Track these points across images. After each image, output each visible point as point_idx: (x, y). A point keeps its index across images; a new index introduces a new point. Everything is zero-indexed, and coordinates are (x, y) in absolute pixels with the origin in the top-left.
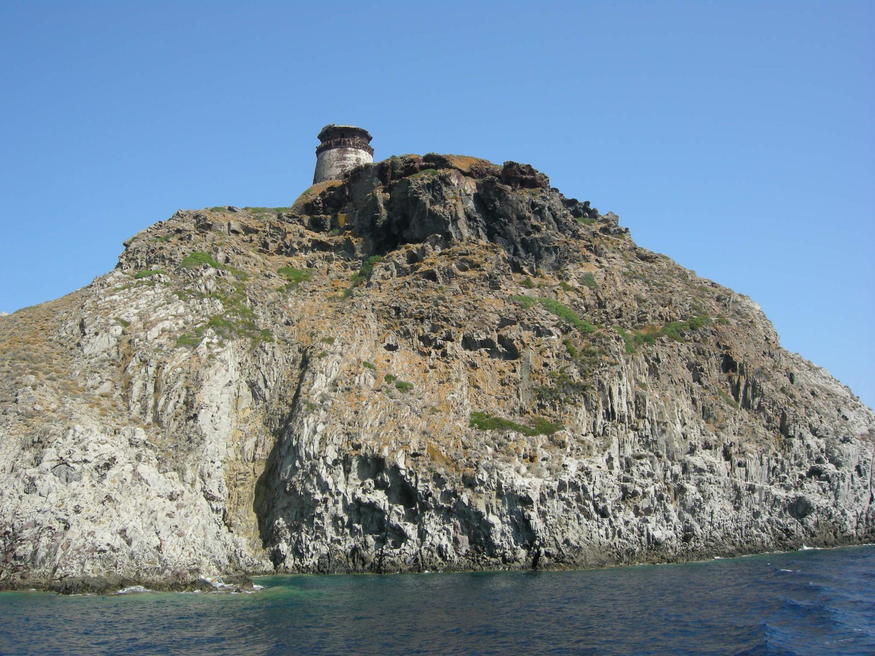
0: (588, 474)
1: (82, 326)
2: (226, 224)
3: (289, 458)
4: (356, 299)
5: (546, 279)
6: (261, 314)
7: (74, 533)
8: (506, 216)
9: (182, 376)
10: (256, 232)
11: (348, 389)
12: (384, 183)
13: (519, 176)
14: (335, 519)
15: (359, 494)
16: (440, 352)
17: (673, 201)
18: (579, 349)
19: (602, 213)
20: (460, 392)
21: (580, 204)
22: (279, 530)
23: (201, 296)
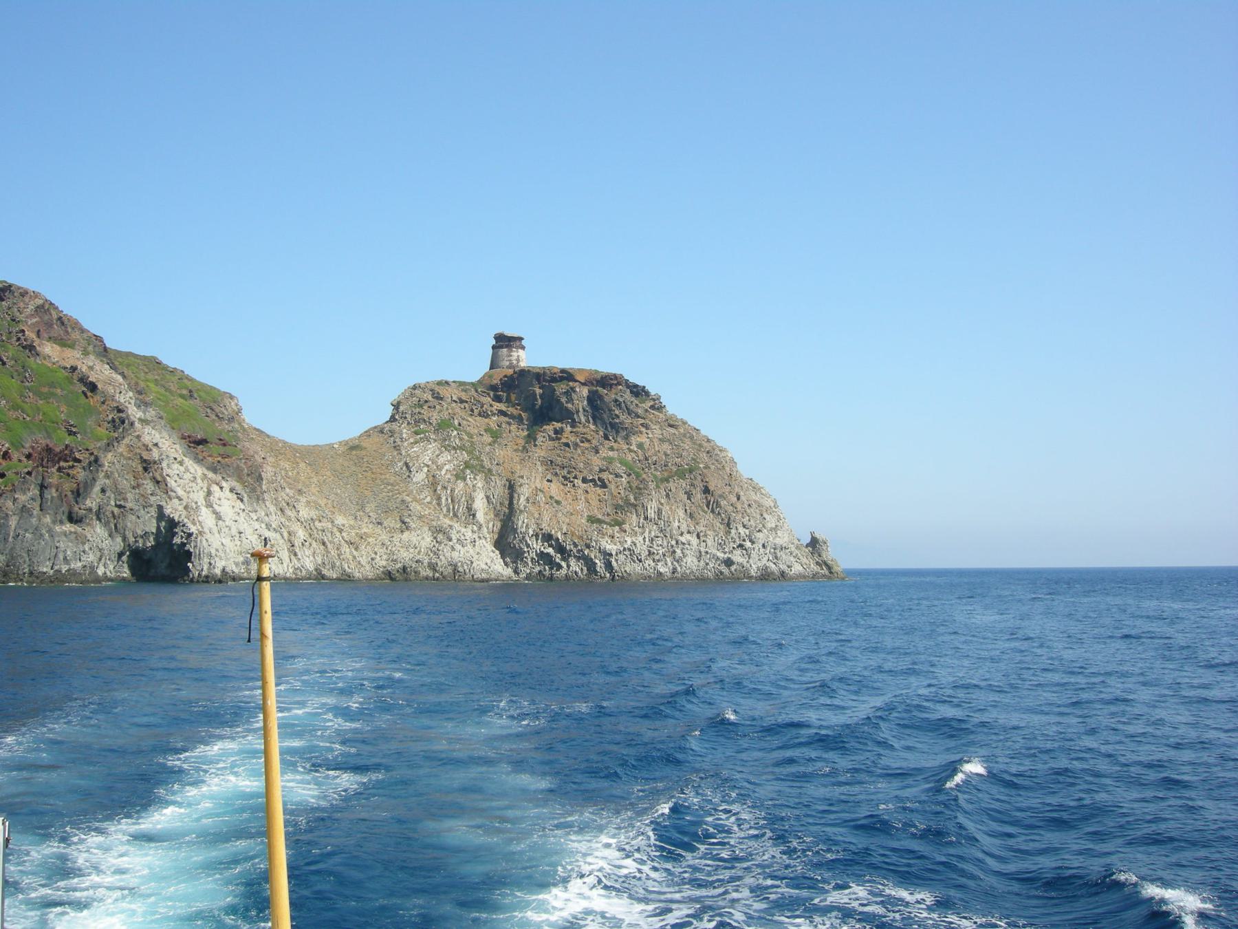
1: (406, 464)
13: (608, 381)
17: (695, 386)
18: (634, 486)
19: (653, 392)
20: (581, 506)
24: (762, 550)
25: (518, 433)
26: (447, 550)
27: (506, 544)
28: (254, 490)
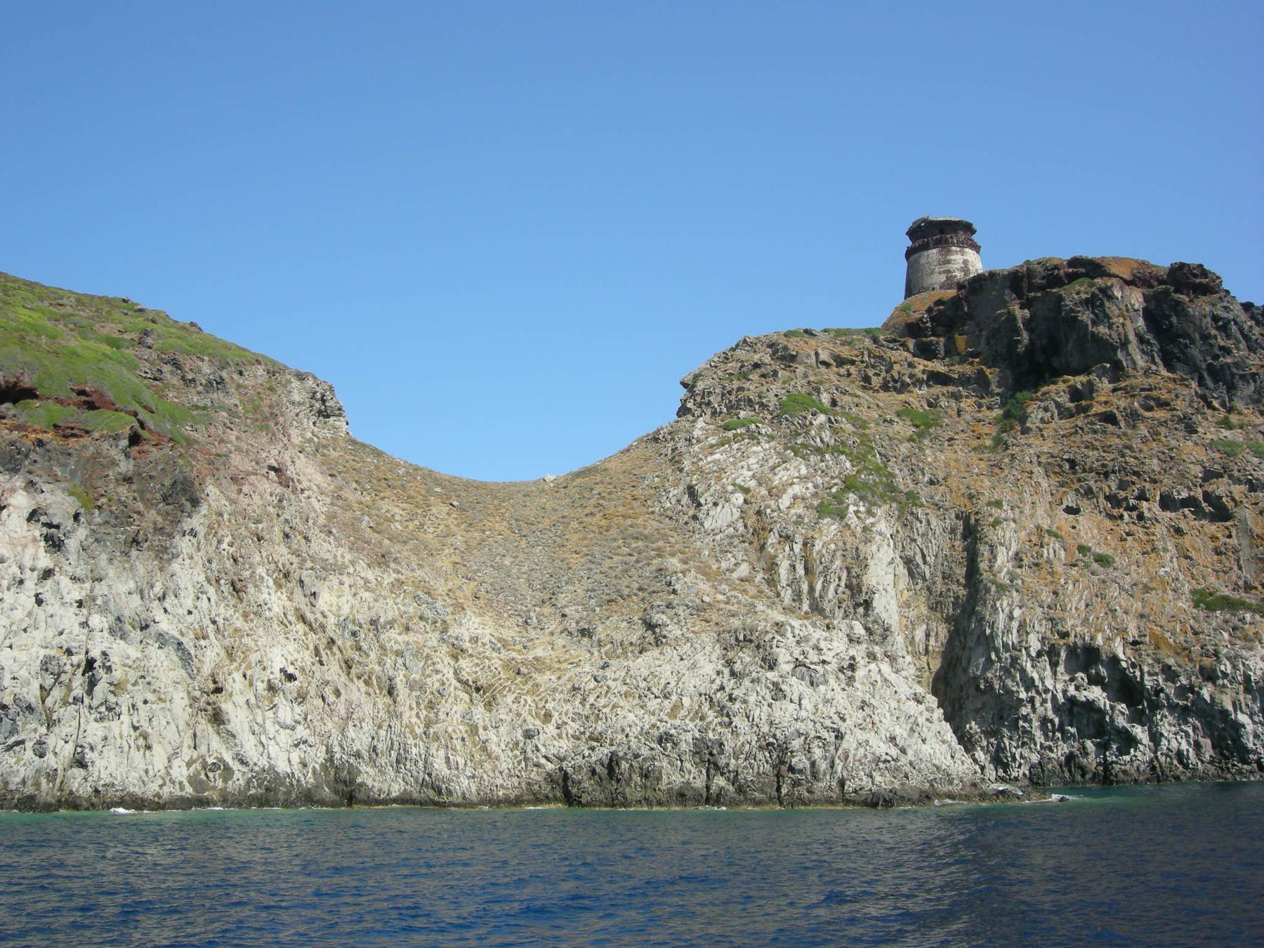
1: (691, 492)
2: (813, 353)
3: (980, 650)
5: (1246, 416)
6: (897, 472)
7: (849, 743)
8: (1187, 336)
9: (839, 554)
11: (1037, 565)
12: (1019, 297)
13: (1190, 280)
14: (1044, 721)
15: (1072, 691)
16: (1134, 514)
20: (1169, 565)
21: (1257, 308)
22: (972, 736)
25: (973, 414)
26: (753, 695)
27: (966, 686)
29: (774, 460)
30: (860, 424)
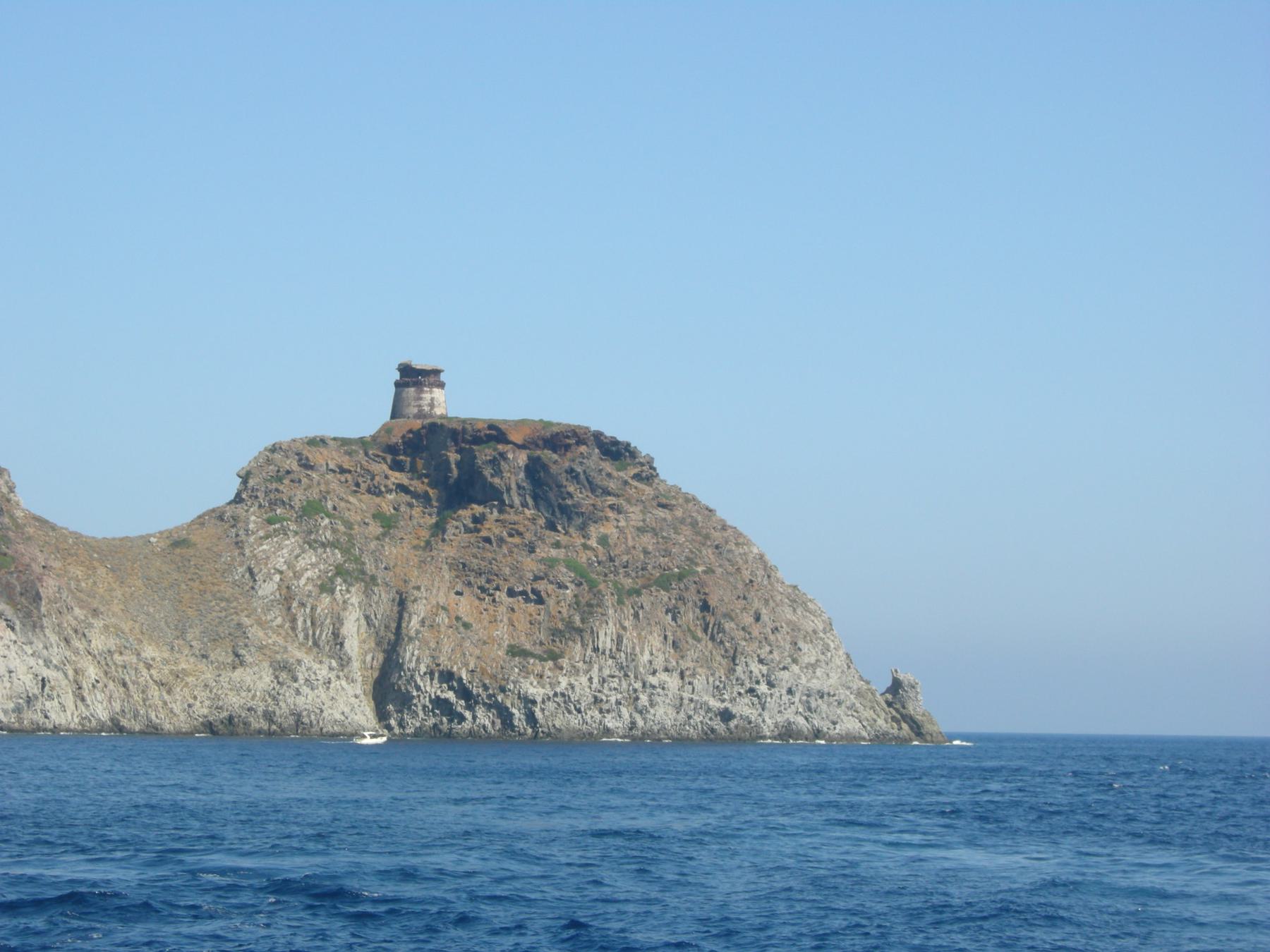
0: (573, 688)
1: (250, 570)
4: (434, 553)
7: (325, 714)
8: (548, 485)
10: (350, 472)
12: (456, 444)
13: (560, 440)
14: (424, 707)
15: (439, 693)
18: (583, 601)
23: (323, 545)
24: (785, 698)
25: (422, 518)
27: (388, 691)
28: (28, 615)
29: (297, 551)
30: (349, 525)
